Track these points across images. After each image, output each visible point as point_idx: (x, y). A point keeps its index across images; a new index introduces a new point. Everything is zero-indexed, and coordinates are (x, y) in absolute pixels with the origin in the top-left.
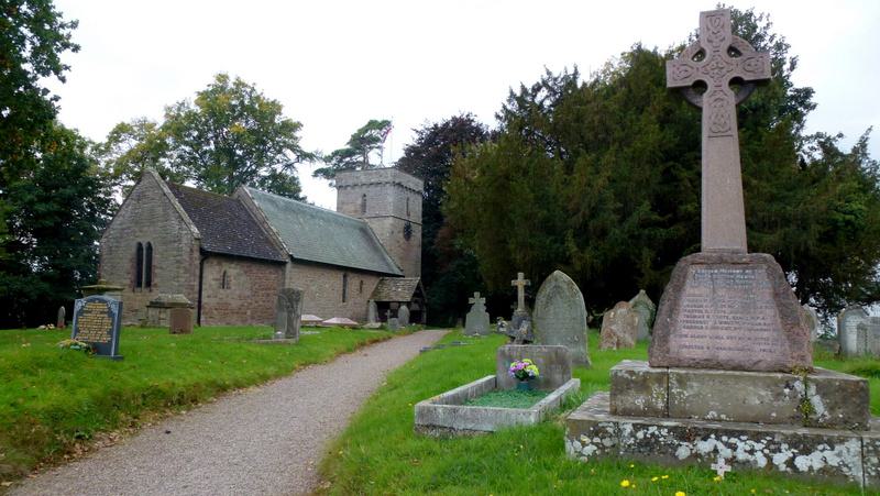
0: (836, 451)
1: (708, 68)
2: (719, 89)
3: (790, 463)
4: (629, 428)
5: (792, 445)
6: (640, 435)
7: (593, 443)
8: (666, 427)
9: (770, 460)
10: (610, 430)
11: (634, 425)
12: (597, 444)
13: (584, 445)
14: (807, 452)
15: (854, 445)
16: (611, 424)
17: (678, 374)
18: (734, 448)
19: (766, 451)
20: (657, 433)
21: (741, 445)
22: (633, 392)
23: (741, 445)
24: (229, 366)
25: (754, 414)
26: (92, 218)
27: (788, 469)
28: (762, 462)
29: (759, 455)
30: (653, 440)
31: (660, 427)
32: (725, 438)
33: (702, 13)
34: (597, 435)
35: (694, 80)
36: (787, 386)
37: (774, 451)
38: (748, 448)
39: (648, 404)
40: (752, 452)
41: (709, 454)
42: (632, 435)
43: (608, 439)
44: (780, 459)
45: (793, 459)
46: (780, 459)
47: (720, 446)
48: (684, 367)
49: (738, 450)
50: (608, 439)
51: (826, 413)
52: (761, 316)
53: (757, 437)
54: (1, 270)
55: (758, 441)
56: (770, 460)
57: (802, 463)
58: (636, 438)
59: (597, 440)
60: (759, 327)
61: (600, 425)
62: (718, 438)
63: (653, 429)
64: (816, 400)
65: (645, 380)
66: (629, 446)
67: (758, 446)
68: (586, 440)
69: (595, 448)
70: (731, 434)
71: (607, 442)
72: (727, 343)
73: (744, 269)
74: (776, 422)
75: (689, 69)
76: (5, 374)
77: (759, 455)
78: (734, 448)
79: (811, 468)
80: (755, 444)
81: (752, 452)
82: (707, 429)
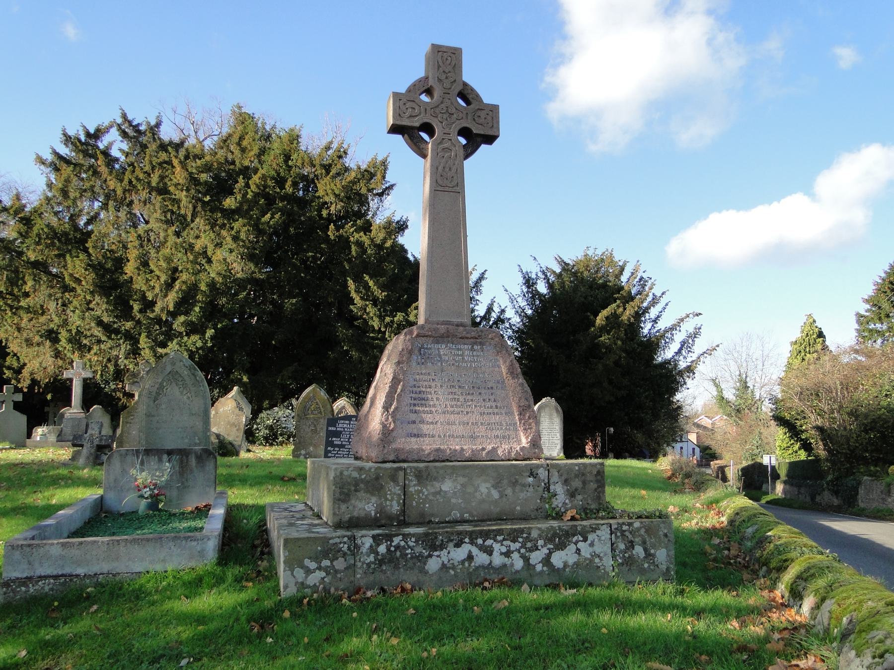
0: (589, 542)
1: (437, 111)
2: (447, 137)
3: (547, 561)
4: (368, 542)
5: (549, 540)
6: (382, 549)
7: (320, 568)
8: (413, 535)
9: (526, 560)
10: (345, 548)
11: (374, 537)
12: (326, 570)
13: (308, 571)
14: (561, 546)
15: (604, 533)
16: (346, 539)
17: (416, 468)
18: (489, 551)
19: (523, 551)
20: (402, 543)
21: (496, 546)
22: (362, 494)
23: (496, 546)
24: (418, 359)
25: (498, 510)
26: (651, 630)
27: (545, 568)
28: (519, 564)
29: (515, 555)
30: (398, 554)
31: (405, 536)
32: (480, 541)
33: (434, 46)
34: (326, 556)
35: (421, 122)
36: (531, 474)
37: (531, 550)
38: (504, 550)
39: (381, 510)
40: (508, 554)
41: (463, 562)
42: (373, 550)
43: (341, 560)
44: (536, 557)
45: (549, 555)
46: (536, 557)
47: (475, 551)
48: (424, 461)
49: (495, 553)
50: (341, 560)
51: (567, 501)
52: (492, 398)
53: (513, 536)
54: (3, 440)
55: (514, 541)
56: (526, 560)
57: (558, 559)
58: (377, 553)
59: (326, 563)
60: (490, 410)
61: (331, 541)
62: (472, 543)
63: (397, 540)
64: (559, 488)
65: (377, 478)
66: (369, 565)
67: (515, 546)
68: (313, 565)
69: (323, 574)
70: (486, 535)
71: (340, 564)
72: (459, 430)
73: (473, 344)
74: (525, 518)
75: (417, 108)
76: (1, 450)
77: (515, 555)
78: (489, 551)
79: (566, 565)
80: (512, 544)
81: (508, 554)
82: (459, 533)
